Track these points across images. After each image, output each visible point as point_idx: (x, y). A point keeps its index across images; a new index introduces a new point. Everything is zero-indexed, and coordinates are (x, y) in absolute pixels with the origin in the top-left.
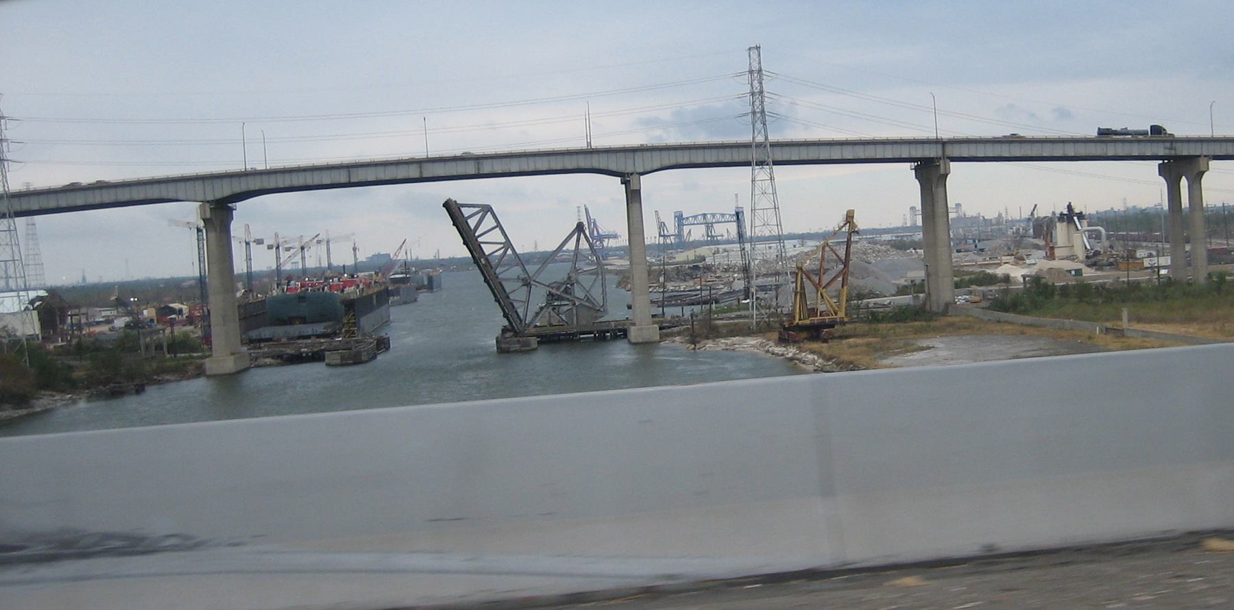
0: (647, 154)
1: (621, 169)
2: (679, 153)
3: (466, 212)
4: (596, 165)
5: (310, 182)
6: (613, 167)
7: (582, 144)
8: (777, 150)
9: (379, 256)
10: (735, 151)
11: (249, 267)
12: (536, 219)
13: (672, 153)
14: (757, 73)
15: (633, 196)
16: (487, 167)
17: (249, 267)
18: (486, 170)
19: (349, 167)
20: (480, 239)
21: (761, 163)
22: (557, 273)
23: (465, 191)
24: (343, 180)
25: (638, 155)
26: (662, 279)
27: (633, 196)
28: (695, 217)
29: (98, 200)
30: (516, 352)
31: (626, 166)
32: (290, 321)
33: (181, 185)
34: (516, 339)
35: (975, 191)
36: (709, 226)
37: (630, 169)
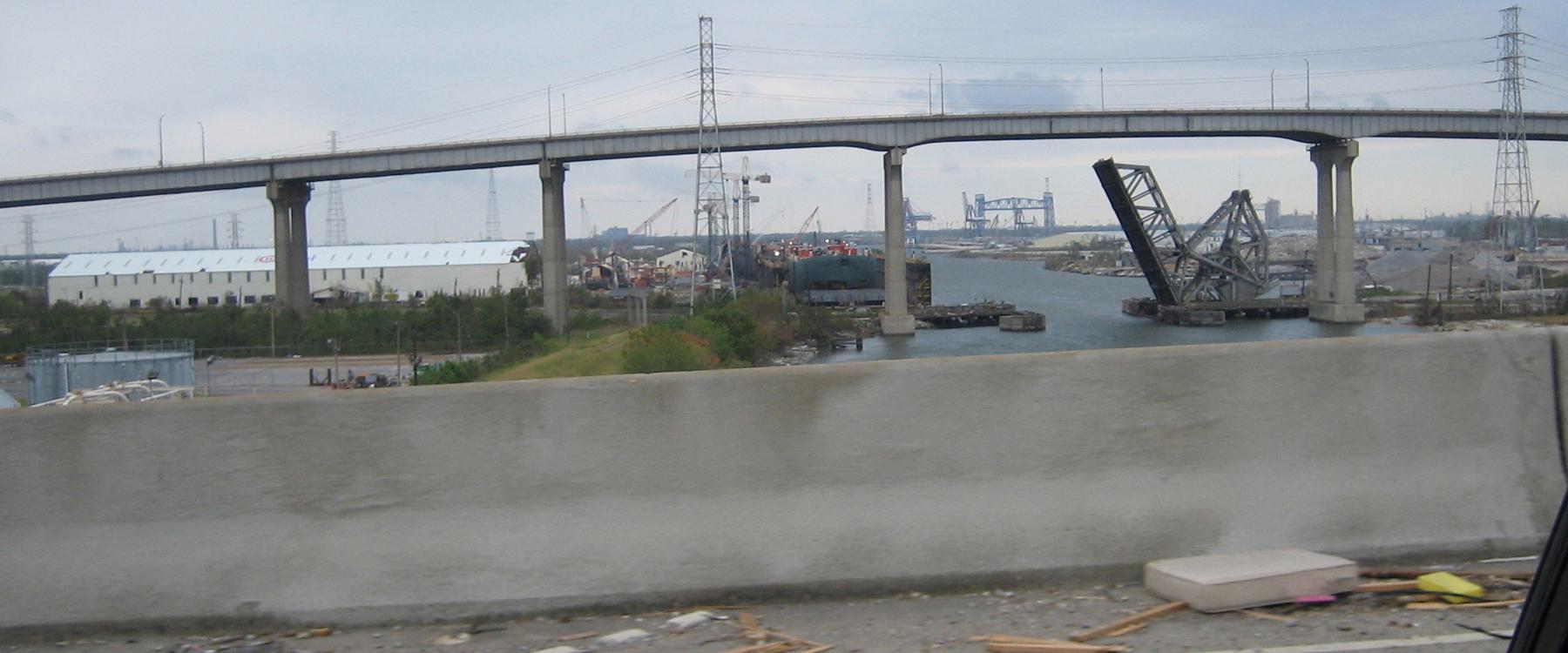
0: (1366, 119)
1: (882, 142)
2: (1236, 119)
3: (1122, 173)
4: (854, 138)
5: (1008, 131)
6: (872, 140)
7: (1300, 105)
8: (1530, 122)
9: (615, 230)
10: (1458, 120)
11: (29, 242)
12: (1192, 184)
13: (928, 125)
14: (1511, 36)
15: (893, 172)
16: (1196, 125)
17: (29, 242)
18: (1196, 127)
19: (1188, 115)
20: (1136, 203)
21: (1512, 137)
22: (1208, 245)
23: (1123, 152)
24: (1044, 130)
25: (1356, 121)
26: (1119, 263)
27: (893, 172)
28: (998, 201)
29: (813, 139)
30: (1208, 326)
31: (888, 140)
32: (830, 286)
33: (872, 128)
34: (997, 317)
35: (603, 202)
36: (1018, 212)
37: (890, 143)
